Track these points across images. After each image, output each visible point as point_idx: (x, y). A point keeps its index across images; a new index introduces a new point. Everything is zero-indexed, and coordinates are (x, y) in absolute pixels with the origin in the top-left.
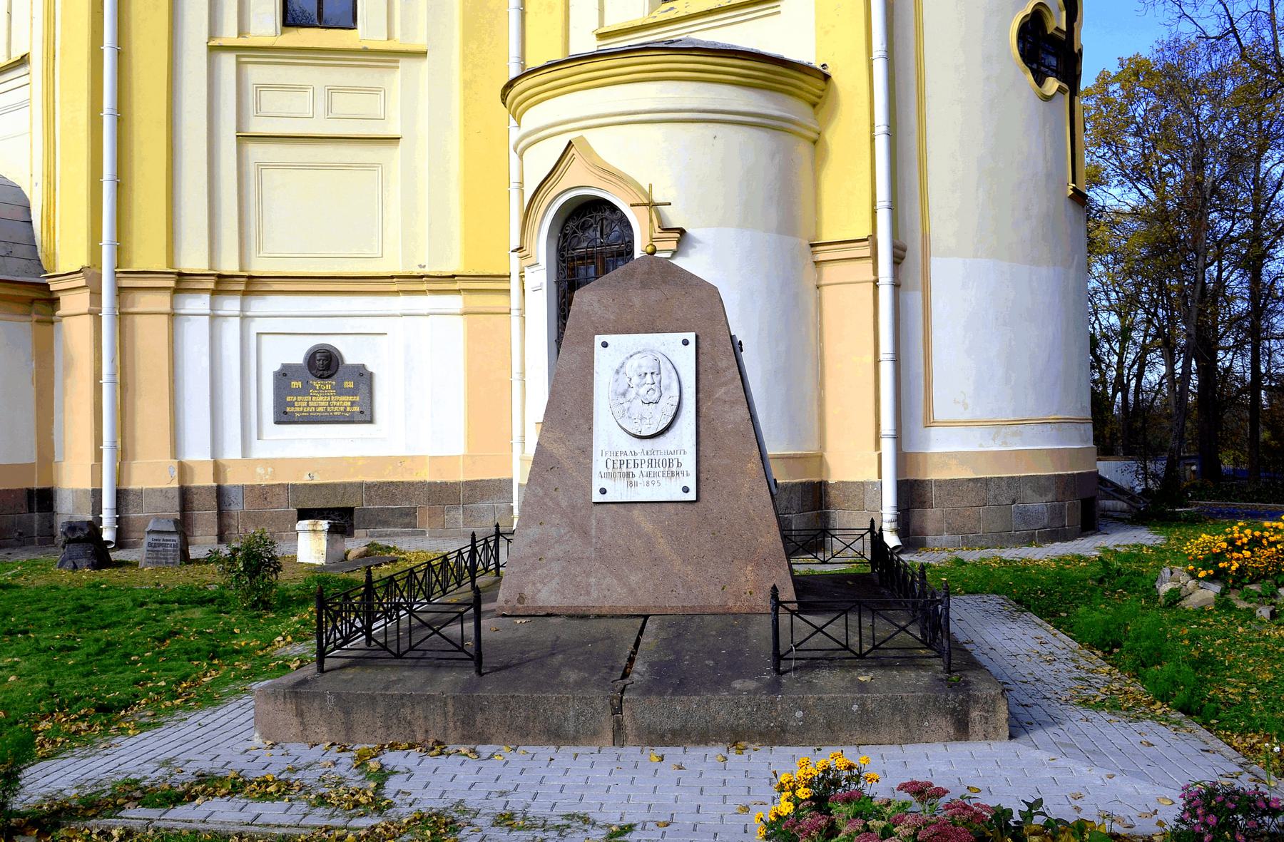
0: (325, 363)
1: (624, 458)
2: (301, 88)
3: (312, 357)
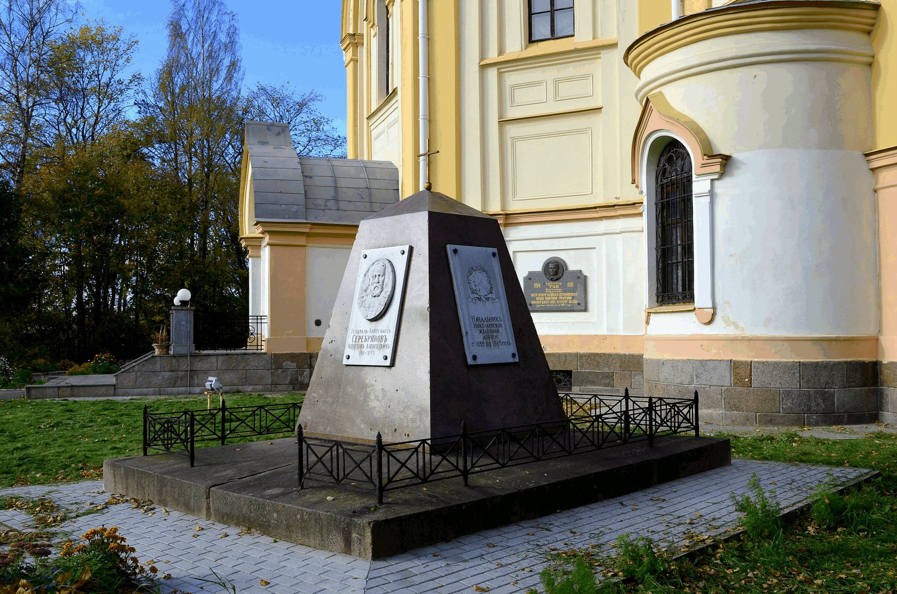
0: (554, 270)
1: (361, 335)
2: (537, 83)
3: (546, 266)
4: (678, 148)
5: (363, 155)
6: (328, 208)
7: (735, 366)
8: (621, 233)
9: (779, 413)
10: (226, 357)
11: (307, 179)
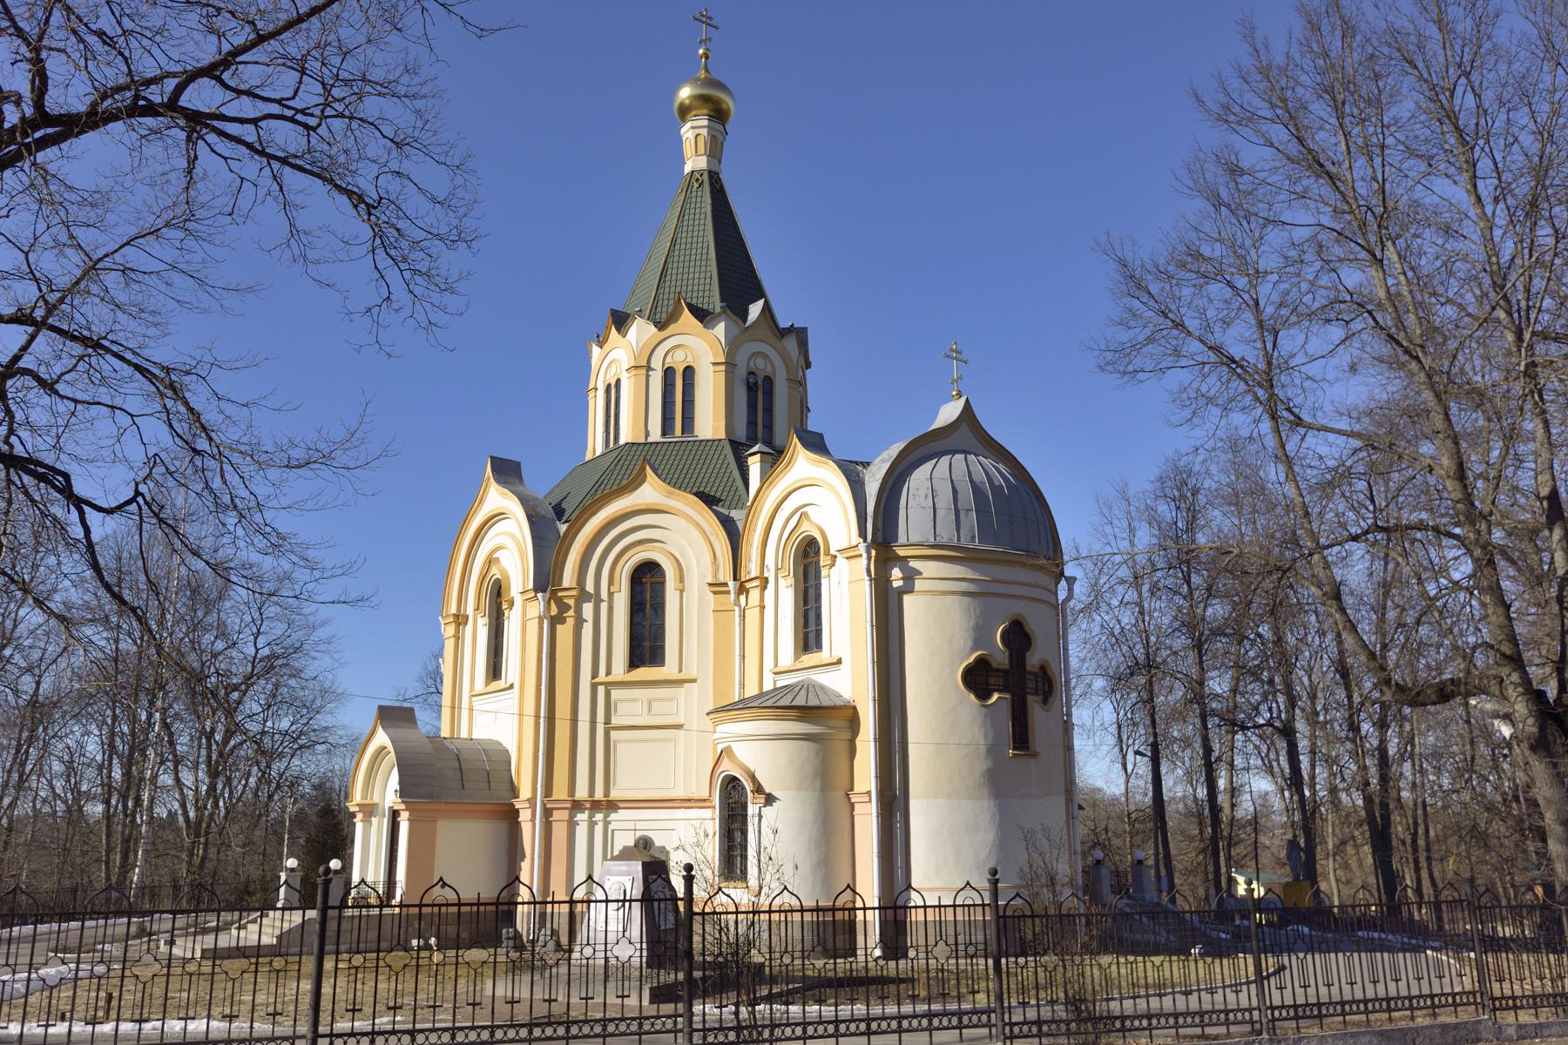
2: (635, 700)
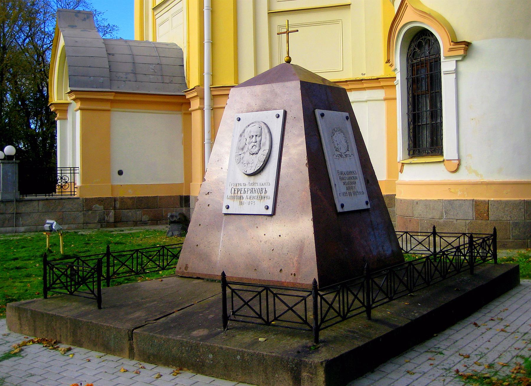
1: (240, 187)
4: (426, 36)
5: (147, 36)
6: (128, 80)
7: (476, 204)
8: (366, 101)
9: (510, 239)
10: (46, 202)
11: (111, 56)
